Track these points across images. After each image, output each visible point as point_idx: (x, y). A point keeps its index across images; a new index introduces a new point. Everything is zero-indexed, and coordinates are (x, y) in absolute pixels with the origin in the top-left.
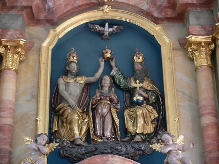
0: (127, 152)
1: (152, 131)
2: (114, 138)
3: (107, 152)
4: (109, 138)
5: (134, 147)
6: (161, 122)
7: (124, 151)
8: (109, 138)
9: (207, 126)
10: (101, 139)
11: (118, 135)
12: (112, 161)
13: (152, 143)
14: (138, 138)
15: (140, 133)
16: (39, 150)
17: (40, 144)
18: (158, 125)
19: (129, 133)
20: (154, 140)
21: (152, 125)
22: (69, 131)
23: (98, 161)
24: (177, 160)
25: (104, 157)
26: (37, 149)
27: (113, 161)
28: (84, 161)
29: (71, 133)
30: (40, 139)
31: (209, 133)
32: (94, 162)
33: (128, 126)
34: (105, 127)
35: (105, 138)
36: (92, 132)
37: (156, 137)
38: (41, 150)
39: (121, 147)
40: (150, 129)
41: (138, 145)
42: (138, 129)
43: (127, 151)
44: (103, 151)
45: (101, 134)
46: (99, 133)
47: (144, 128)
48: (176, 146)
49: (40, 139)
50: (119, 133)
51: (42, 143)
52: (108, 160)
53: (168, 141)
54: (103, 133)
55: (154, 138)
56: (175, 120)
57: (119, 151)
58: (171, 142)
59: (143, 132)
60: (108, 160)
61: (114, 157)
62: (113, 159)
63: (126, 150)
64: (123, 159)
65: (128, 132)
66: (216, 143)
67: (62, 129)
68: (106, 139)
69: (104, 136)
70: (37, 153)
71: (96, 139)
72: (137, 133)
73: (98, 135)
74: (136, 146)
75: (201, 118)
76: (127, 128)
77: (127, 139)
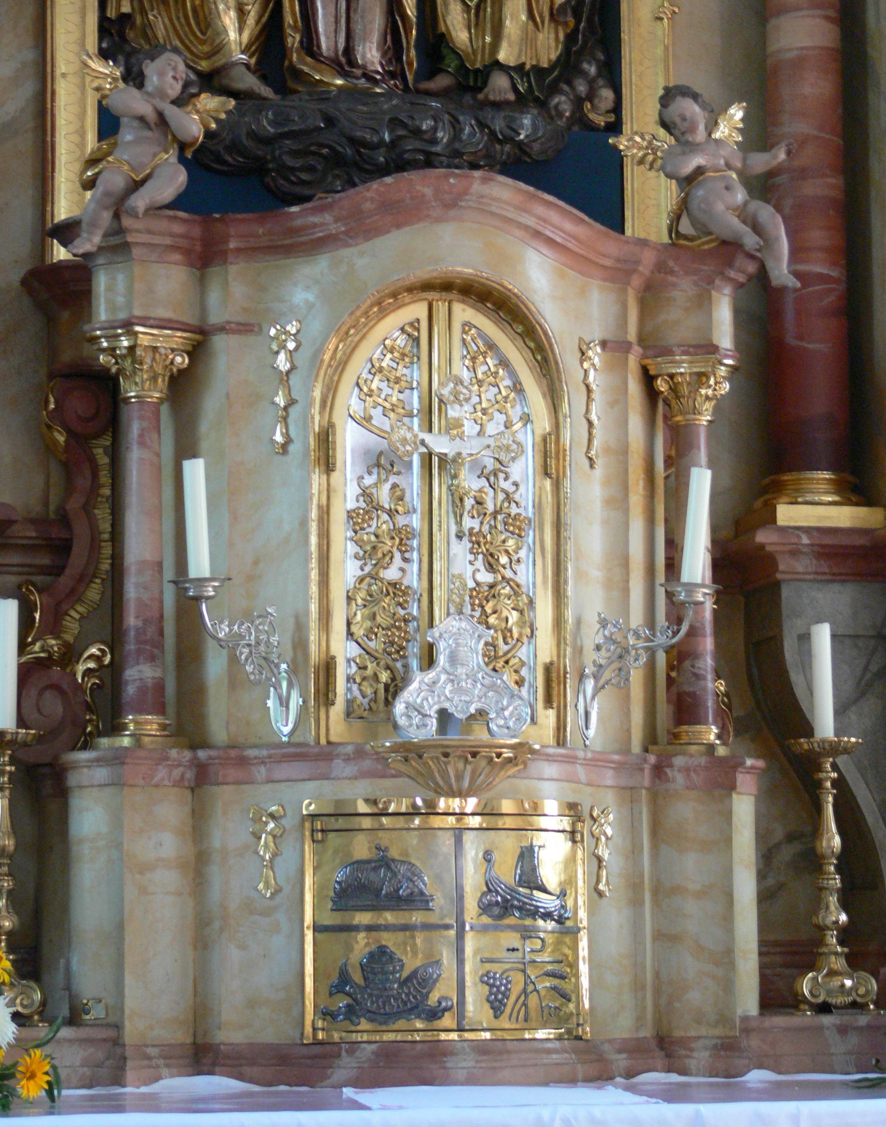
0: (457, 145)
1: (553, 56)
2: (392, 75)
3: (375, 140)
4: (378, 77)
5: (489, 128)
6: (590, 21)
7: (445, 140)
8: (378, 77)
9: (798, 63)
10: (344, 75)
11: (410, 64)
12: (482, 197)
13: (553, 113)
14: (500, 84)
15: (512, 65)
16: (162, 121)
17: (161, 93)
18: (576, 30)
19: (452, 56)
20: (563, 98)
21: (552, 31)
22: (189, 24)
23: (423, 195)
24: (728, 208)
25: (452, 181)
26: (151, 116)
27: (484, 200)
28: (368, 190)
29: (203, 34)
30: (162, 74)
31: (807, 90)
32: (408, 195)
33: (449, 23)
34: (357, 28)
35: (358, 72)
36: (293, 39)
37: (569, 83)
38: (173, 124)
39: (436, 121)
40: (548, 47)
41: (505, 118)
42: (504, 45)
43: (461, 140)
44: (359, 134)
45: (336, 51)
46: (328, 39)
47: (527, 41)
48: (722, 152)
49: (162, 74)
50: (413, 53)
51: (170, 91)
52: (466, 192)
53: (693, 129)
54: (349, 51)
55: (561, 92)
56: (661, 19)
57: (425, 137)
58: (701, 135)
59: (523, 59)
60: (467, 194)
61: (492, 183)
62: (485, 189)
63: (456, 137)
64: (527, 192)
65: (445, 51)
66: (833, 138)
67: (155, 12)
68: (363, 81)
69: (352, 63)
70: (149, 134)
71: (320, 72)
72: (497, 62)
73: (322, 55)
74: (498, 124)
75: (773, 22)
76: (443, 35)
77: (442, 82)
